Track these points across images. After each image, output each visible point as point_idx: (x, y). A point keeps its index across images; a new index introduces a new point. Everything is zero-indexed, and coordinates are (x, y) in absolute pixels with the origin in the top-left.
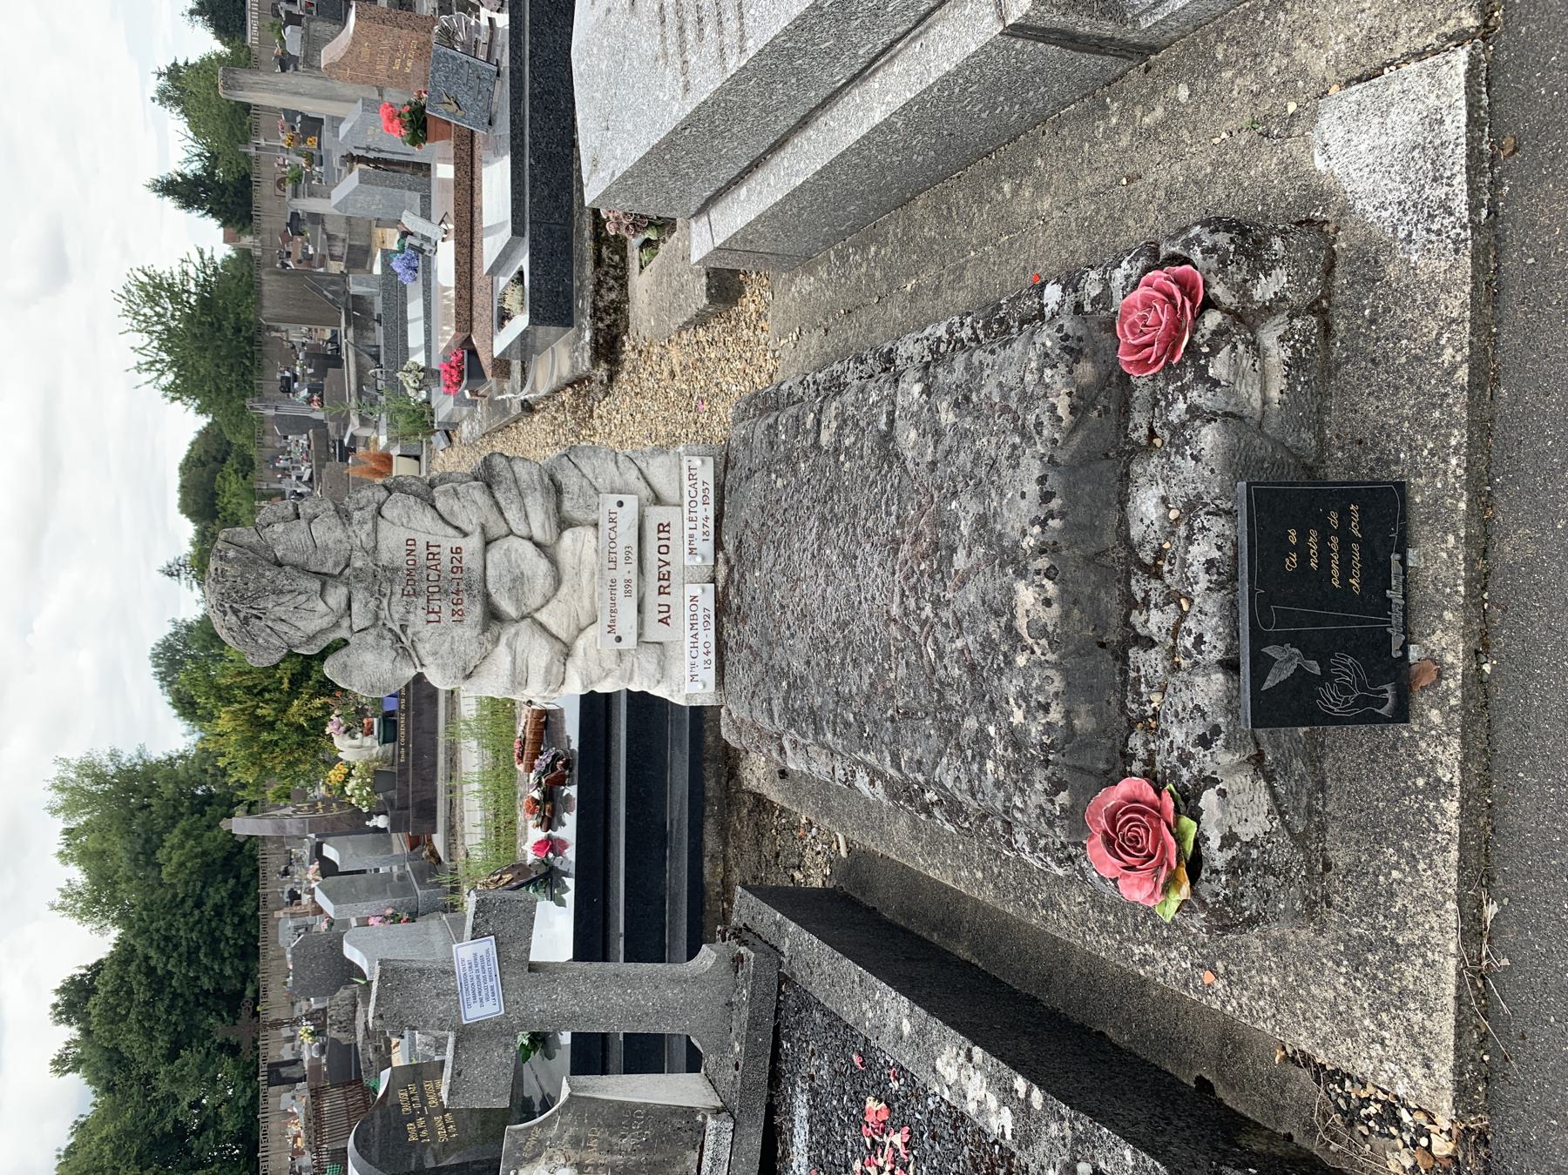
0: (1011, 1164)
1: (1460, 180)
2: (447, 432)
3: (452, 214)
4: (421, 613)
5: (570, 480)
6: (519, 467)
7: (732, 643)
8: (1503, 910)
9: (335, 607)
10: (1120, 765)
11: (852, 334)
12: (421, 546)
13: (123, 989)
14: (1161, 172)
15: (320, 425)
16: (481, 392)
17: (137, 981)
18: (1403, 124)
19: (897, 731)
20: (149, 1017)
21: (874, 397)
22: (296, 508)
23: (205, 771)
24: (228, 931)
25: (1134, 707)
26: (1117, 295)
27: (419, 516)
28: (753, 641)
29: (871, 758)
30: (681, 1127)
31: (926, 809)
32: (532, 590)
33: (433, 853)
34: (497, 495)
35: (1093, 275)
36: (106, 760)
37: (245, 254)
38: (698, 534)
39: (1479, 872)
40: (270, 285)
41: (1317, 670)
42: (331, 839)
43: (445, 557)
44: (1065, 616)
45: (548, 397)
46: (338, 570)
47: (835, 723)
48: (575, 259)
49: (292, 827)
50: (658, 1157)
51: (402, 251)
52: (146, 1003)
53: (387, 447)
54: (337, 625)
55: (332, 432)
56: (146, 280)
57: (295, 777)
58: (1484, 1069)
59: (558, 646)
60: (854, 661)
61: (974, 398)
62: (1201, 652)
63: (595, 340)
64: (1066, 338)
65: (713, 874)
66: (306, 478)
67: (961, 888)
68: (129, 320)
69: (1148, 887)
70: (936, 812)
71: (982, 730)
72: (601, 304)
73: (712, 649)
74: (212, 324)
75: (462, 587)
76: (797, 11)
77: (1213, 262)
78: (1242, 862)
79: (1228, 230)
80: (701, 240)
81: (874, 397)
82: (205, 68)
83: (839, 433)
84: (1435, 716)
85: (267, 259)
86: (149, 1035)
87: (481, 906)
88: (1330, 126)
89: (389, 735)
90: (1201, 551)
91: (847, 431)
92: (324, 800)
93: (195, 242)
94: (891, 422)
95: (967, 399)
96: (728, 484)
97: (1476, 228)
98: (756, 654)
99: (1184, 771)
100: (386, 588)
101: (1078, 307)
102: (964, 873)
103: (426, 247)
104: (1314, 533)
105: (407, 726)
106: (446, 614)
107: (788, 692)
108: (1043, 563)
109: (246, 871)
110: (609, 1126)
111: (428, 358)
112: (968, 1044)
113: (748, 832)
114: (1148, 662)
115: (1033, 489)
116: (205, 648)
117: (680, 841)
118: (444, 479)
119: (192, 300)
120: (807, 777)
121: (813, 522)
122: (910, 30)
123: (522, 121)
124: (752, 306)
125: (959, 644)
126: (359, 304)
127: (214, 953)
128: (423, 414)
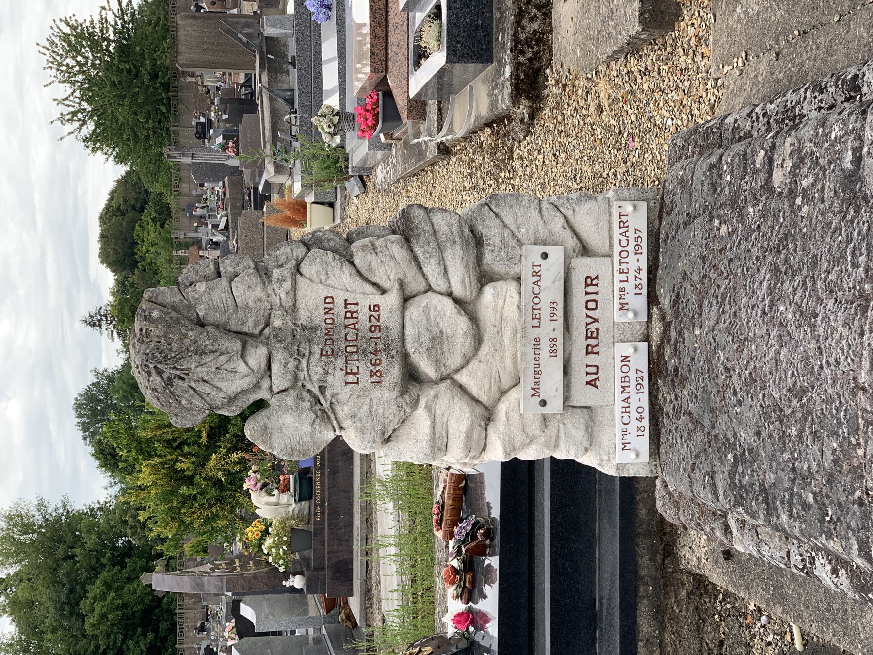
2: (361, 177)
4: (339, 374)
5: (491, 231)
7: (668, 408)
11: (808, 57)
12: (339, 304)
15: (235, 172)
16: (396, 135)
21: (836, 132)
22: (217, 267)
23: (126, 522)
27: (337, 272)
29: (834, 545)
32: (452, 350)
33: (350, 617)
34: (418, 250)
36: (33, 510)
38: (630, 287)
40: (186, 30)
42: (247, 598)
43: (363, 315)
45: (465, 138)
47: (791, 504)
49: (210, 584)
53: (302, 195)
54: (257, 386)
55: (247, 179)
56: (68, 30)
57: (213, 532)
59: (479, 410)
60: (814, 434)
63: (515, 75)
66: (222, 226)
68: (54, 72)
72: (522, 36)
73: (646, 414)
74: (129, 71)
75: (380, 346)
81: (836, 132)
89: (305, 493)
91: (804, 170)
92: (241, 556)
94: (858, 160)
96: (663, 231)
98: (696, 422)
105: (323, 484)
106: (364, 375)
107: (735, 465)
109: (164, 626)
111: (342, 101)
116: (125, 398)
118: (361, 234)
119: (111, 48)
120: (758, 561)
121: (764, 274)
124: (691, 31)
126: (272, 48)
128: (337, 160)
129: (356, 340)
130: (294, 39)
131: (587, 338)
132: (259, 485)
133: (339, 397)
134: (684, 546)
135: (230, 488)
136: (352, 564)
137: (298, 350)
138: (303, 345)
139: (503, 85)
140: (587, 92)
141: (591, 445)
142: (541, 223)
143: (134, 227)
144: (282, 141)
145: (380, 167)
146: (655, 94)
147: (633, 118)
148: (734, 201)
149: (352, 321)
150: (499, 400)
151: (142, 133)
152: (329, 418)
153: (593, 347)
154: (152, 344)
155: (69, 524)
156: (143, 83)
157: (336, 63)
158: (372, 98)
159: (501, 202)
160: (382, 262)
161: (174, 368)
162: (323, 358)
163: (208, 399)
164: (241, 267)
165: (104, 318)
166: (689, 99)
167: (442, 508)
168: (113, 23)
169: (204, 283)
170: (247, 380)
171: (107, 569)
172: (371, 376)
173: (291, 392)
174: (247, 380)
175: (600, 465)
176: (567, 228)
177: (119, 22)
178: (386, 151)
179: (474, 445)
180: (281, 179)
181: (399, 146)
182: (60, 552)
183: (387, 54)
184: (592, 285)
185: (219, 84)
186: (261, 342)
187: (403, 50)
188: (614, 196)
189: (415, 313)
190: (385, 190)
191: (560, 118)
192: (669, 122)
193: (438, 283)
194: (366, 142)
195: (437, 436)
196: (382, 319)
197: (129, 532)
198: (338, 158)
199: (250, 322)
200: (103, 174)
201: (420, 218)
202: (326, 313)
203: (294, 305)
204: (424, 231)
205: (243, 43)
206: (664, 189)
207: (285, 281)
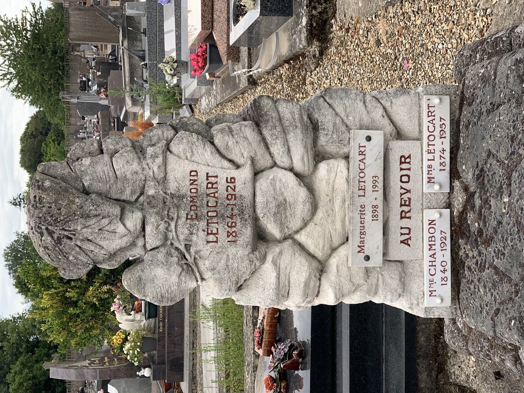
4: (202, 234)
5: (326, 118)
9: (132, 229)
12: (202, 176)
16: (217, 74)
22: (100, 145)
27: (200, 150)
32: (293, 215)
34: (265, 132)
38: (436, 164)
40: (75, 18)
43: (222, 185)
45: (268, 73)
46: (135, 197)
53: (150, 118)
54: (133, 244)
59: (315, 264)
63: (310, 24)
73: (449, 267)
74: (39, 49)
75: (236, 212)
119: (28, 35)
129: (215, 207)
130: (145, 18)
131: (401, 205)
132: (121, 308)
133: (201, 253)
134: (454, 365)
136: (183, 360)
137: (168, 214)
138: (172, 210)
139: (300, 31)
140: (368, 31)
141: (403, 292)
142: (365, 112)
143: (41, 145)
145: (204, 98)
146: (427, 27)
147: (407, 46)
149: (212, 191)
150: (330, 255)
151: (47, 87)
152: (193, 270)
153: (406, 213)
154: (44, 209)
156: (47, 56)
158: (202, 48)
159: (334, 95)
160: (237, 142)
161: (63, 229)
162: (189, 221)
163: (91, 255)
164: (121, 145)
165: (22, 200)
166: (459, 28)
168: (30, 20)
169: (89, 158)
170: (125, 239)
171: (23, 355)
172: (228, 236)
173: (162, 249)
174: (125, 239)
175: (410, 308)
176: (386, 117)
177: (33, 19)
178: (209, 86)
179: (310, 292)
180: (137, 109)
181: (218, 82)
183: (213, 17)
184: (405, 162)
185: (95, 56)
186: (137, 208)
187: (224, 15)
188: (423, 91)
189: (264, 184)
190: (207, 113)
191: (344, 52)
192: (440, 46)
193: (282, 159)
194: (196, 80)
195: (281, 285)
196: (237, 190)
197: (37, 332)
198: (175, 93)
200: (23, 112)
201: (269, 106)
202: (191, 184)
203: (165, 177)
204: (272, 117)
205: (111, 22)
206: (463, 85)
207: (157, 157)
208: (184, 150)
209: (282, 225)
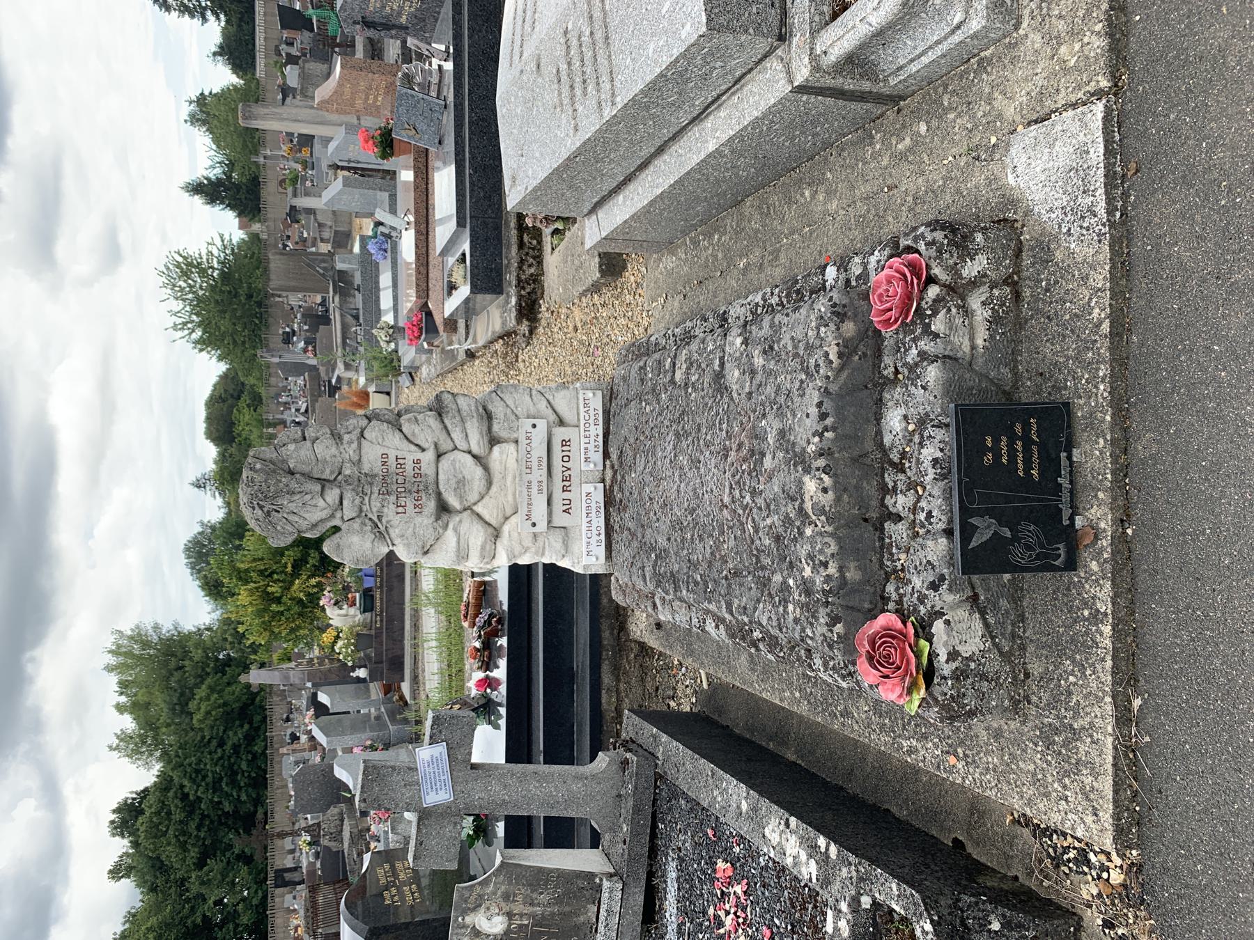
0: (816, 901)
1: (1101, 191)
3: (413, 210)
4: (392, 507)
5: (497, 409)
6: (461, 400)
7: (616, 527)
8: (1145, 702)
10: (880, 605)
11: (702, 298)
12: (392, 460)
13: (163, 810)
14: (911, 184)
15: (314, 369)
17: (175, 805)
18: (1064, 154)
19: (729, 586)
20: (184, 833)
21: (710, 347)
23: (226, 639)
24: (244, 766)
25: (889, 563)
26: (872, 273)
27: (390, 437)
28: (631, 525)
29: (712, 607)
30: (583, 887)
31: (754, 644)
32: (471, 490)
33: (402, 698)
34: (446, 421)
35: (857, 260)
36: (150, 632)
37: (255, 238)
38: (591, 447)
39: (1127, 675)
40: (276, 263)
41: (1008, 534)
44: (838, 500)
45: (485, 347)
47: (688, 583)
48: (503, 248)
49: (295, 678)
50: (567, 909)
51: (375, 236)
52: (181, 822)
53: (366, 386)
54: (332, 516)
55: (323, 374)
56: (180, 260)
57: (297, 640)
58: (1136, 816)
59: (490, 530)
60: (700, 536)
61: (776, 347)
62: (931, 524)
63: (519, 304)
64: (835, 305)
65: (609, 703)
66: (303, 410)
67: (785, 705)
68: (169, 291)
69: (898, 690)
70: (761, 646)
71: (785, 582)
74: (230, 292)
75: (421, 488)
76: (649, 79)
77: (933, 252)
78: (963, 672)
79: (943, 229)
80: (592, 232)
81: (710, 347)
82: (224, 96)
83: (687, 372)
84: (1094, 566)
85: (272, 241)
86: (183, 847)
87: (436, 720)
88: (1017, 154)
89: (368, 607)
90: (929, 452)
93: (219, 229)
94: (722, 365)
95: (771, 348)
97: (1112, 225)
98: (633, 535)
99: (922, 608)
100: (367, 489)
101: (848, 281)
102: (787, 694)
103: (394, 234)
104: (1004, 439)
105: (381, 599)
107: (656, 561)
108: (821, 462)
109: (257, 718)
110: (531, 885)
111: (396, 317)
112: (787, 815)
113: (634, 671)
114: (897, 532)
115: (814, 411)
117: (584, 679)
118: (407, 411)
121: (671, 437)
122: (730, 88)
123: (463, 142)
124: (632, 278)
125: (769, 521)
126: (343, 276)
127: (233, 783)
128: (392, 361)
135: (309, 607)
144: (350, 346)
148: (654, 390)
155: (180, 641)
157: (391, 290)
167: (467, 605)
182: (173, 664)
193: (462, 444)
197: (228, 646)
199: (328, 471)
200: (208, 370)
208: (377, 437)
209: (461, 498)
